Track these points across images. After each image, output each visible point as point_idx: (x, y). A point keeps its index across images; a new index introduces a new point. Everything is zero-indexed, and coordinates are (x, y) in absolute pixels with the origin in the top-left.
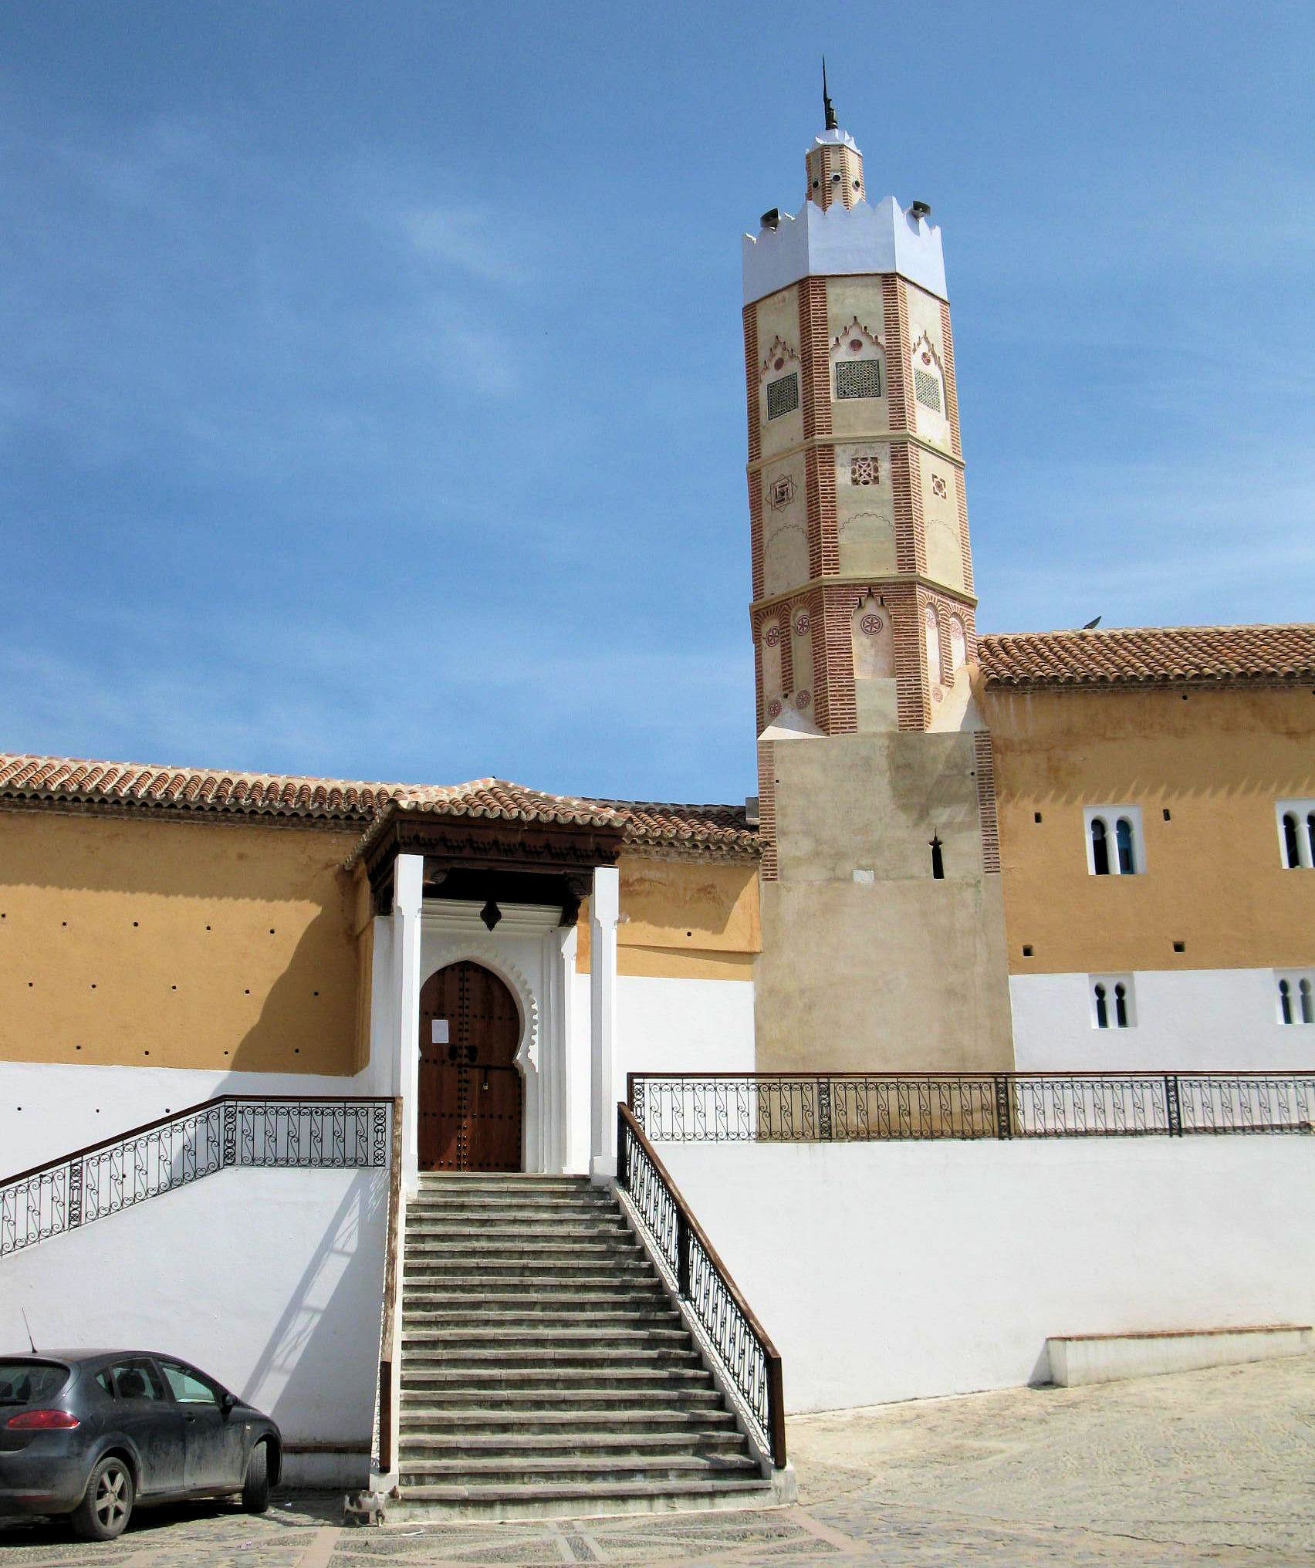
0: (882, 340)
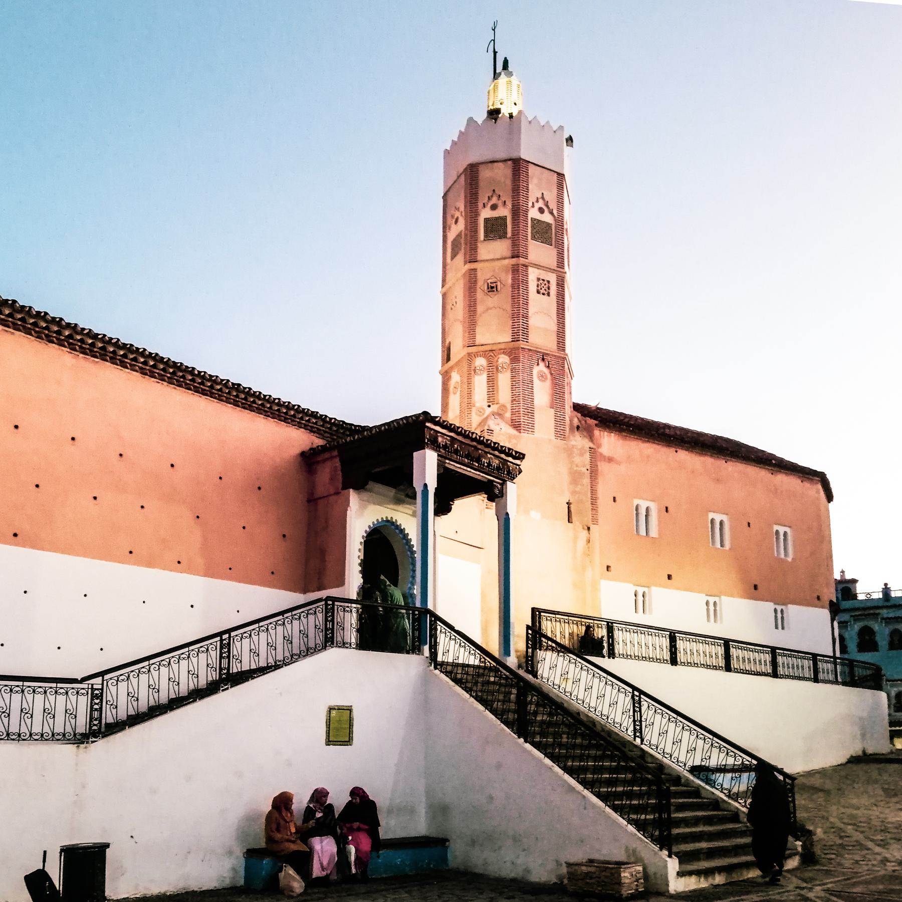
0: (555, 212)
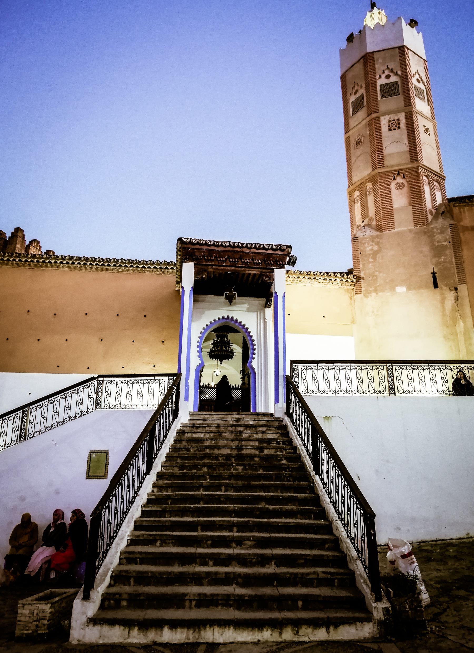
0: (399, 73)
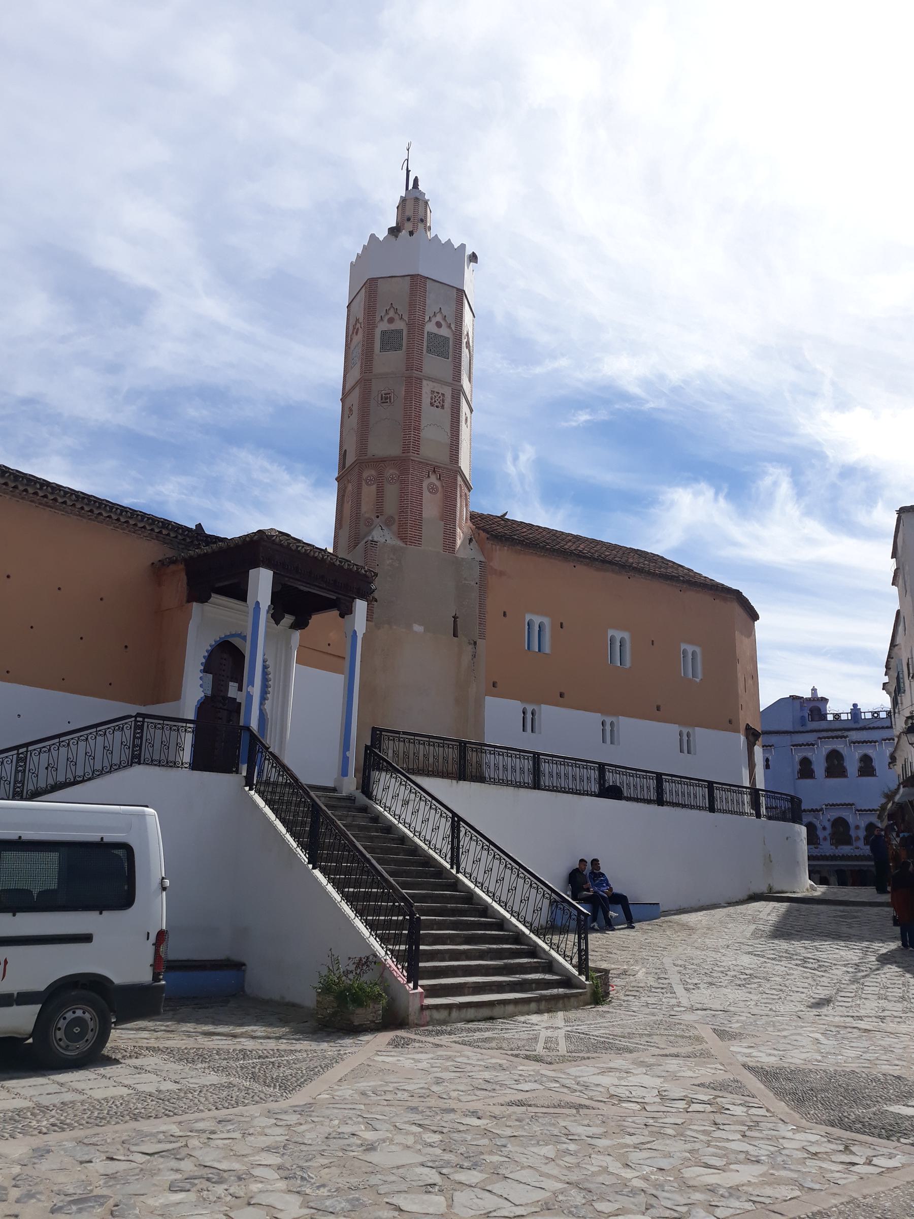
0: (453, 326)
